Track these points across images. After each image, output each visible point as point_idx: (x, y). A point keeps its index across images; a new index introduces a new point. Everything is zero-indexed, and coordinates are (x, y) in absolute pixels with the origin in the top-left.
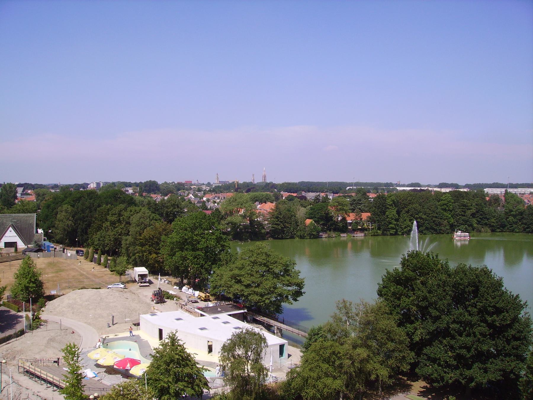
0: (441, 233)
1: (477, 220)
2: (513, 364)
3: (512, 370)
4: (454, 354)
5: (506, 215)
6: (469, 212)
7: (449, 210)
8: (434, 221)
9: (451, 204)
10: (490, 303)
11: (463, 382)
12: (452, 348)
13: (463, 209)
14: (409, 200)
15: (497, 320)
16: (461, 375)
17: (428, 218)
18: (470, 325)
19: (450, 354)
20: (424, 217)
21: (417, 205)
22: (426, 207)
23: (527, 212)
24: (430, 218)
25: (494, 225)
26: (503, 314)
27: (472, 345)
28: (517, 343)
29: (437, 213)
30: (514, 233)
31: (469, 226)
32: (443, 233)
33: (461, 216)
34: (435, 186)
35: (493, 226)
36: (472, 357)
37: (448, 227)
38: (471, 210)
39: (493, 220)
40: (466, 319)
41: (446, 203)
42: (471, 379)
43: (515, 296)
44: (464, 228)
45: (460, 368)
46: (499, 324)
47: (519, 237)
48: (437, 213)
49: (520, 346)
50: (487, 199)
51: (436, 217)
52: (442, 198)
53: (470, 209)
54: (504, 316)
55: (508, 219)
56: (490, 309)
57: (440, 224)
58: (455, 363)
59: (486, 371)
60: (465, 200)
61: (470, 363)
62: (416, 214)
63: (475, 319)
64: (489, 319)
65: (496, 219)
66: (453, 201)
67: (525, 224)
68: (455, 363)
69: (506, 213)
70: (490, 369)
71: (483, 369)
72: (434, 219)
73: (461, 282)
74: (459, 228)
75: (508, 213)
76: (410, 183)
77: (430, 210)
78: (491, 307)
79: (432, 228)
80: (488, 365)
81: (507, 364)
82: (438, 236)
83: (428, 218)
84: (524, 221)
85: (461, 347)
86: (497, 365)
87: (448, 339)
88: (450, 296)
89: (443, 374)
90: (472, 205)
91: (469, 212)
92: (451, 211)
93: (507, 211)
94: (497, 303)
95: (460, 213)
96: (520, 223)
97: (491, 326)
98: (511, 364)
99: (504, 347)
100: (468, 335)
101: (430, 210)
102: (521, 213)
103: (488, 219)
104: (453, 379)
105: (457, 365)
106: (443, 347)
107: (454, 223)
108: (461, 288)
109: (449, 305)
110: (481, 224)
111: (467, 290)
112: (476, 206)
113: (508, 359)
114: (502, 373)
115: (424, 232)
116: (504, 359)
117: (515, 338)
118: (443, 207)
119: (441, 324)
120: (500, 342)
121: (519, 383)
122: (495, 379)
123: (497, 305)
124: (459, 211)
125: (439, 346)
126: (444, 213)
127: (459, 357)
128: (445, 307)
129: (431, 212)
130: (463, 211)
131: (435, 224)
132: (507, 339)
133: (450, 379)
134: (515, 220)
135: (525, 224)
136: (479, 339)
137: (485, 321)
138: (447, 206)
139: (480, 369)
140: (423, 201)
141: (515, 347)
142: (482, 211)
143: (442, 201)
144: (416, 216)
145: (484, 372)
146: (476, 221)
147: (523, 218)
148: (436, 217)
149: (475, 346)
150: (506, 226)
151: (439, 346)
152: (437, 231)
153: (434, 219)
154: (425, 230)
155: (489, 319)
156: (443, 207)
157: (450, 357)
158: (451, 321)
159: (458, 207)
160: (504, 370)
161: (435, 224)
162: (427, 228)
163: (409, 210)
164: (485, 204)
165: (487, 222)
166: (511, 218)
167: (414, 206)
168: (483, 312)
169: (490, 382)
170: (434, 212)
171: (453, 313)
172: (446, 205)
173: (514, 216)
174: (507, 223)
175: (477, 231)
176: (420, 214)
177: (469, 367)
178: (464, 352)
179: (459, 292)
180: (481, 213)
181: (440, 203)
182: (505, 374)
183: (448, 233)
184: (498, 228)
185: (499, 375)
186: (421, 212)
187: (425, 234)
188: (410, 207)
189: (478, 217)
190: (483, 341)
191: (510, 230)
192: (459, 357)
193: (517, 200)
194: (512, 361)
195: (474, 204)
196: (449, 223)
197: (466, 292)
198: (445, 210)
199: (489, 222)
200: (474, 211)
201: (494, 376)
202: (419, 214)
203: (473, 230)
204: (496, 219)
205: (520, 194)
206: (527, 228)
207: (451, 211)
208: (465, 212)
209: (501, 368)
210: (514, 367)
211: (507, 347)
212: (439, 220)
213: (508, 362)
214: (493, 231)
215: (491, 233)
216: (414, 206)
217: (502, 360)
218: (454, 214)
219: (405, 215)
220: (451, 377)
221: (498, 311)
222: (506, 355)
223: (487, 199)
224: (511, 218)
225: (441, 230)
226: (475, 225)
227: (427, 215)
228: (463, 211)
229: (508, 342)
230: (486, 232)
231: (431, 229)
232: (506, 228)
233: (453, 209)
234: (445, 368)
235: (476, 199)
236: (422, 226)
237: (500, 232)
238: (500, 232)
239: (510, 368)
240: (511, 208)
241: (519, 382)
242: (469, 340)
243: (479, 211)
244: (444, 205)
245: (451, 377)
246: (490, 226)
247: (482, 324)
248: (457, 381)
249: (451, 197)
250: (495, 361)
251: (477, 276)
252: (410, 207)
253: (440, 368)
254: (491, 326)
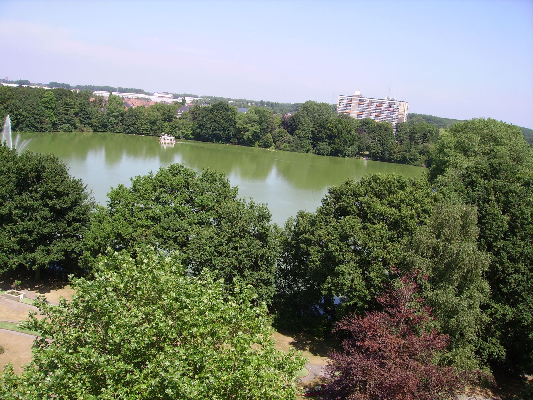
0: (42, 131)
1: (80, 120)
2: (74, 245)
3: (73, 249)
4: (18, 239)
5: (107, 115)
6: (72, 112)
7: (51, 108)
8: (35, 119)
9: (53, 101)
10: (51, 187)
11: (27, 265)
12: (15, 233)
13: (65, 107)
14: (8, 95)
15: (58, 203)
16: (25, 258)
17: (28, 115)
18: (34, 210)
19: (13, 239)
20: (24, 113)
21: (17, 101)
22: (27, 103)
23: (127, 114)
24: (31, 115)
25: (96, 125)
26: (63, 197)
27: (33, 228)
28: (77, 224)
29: (38, 111)
30: (115, 134)
31: (71, 125)
32: (44, 132)
33: (63, 115)
34: (45, 85)
35: (95, 126)
36: (34, 240)
37: (50, 125)
38: (74, 109)
39: (95, 120)
40: (27, 205)
41: (49, 100)
42: (34, 262)
43: (77, 180)
44: (67, 126)
45: (23, 252)
46: (60, 207)
47: (119, 137)
48: (38, 111)
49: (80, 227)
50: (92, 99)
51: (38, 115)
52: (44, 95)
53: (73, 108)
54: (64, 200)
55: (109, 120)
56: (50, 193)
57: (41, 122)
58: (18, 248)
59: (48, 252)
60: (68, 99)
61: (33, 246)
62: (16, 111)
63: (36, 204)
64: (50, 203)
65: (99, 119)
66: (55, 99)
67: (125, 125)
68: (18, 248)
69: (108, 114)
70: (52, 250)
71: (46, 251)
72: (35, 116)
73: (23, 168)
74: (61, 126)
75: (110, 114)
76: (18, 80)
77: (31, 106)
78: (52, 191)
79: (34, 127)
80: (51, 247)
81: (69, 245)
82: (39, 134)
83: (28, 115)
84: (125, 122)
85: (22, 232)
86: (59, 246)
87: (11, 225)
88: (14, 182)
89: (6, 260)
90: (75, 104)
91: (72, 112)
92: (53, 109)
93: (109, 112)
94: (58, 187)
95: (63, 112)
96: (121, 124)
97: (52, 209)
98: (72, 245)
99: (65, 229)
100: (31, 220)
101: (31, 106)
102: (122, 115)
103: (91, 119)
104: (17, 264)
105: (20, 249)
106: (7, 233)
107: (57, 121)
108: (23, 174)
109: (11, 191)
110: (83, 124)
111: (30, 175)
112: (79, 106)
113: (69, 239)
114: (63, 253)
115: (24, 129)
116: (65, 240)
117: (75, 220)
118: (45, 105)
119: (3, 210)
120: (63, 225)
121: (79, 261)
122: (57, 259)
123: (58, 190)
124: (61, 110)
125: (3, 233)
126: (46, 111)
127: (21, 242)
128: (7, 193)
129: (32, 109)
130: (66, 110)
131: (37, 122)
132: (68, 221)
133: (14, 264)
134: (116, 121)
135: (125, 125)
136: (40, 222)
137: (46, 205)
138: (50, 104)
139: (43, 251)
140: (24, 97)
141: (75, 228)
142: (85, 111)
143: (45, 98)
144: (16, 112)
145: (47, 254)
146: (79, 121)
147: (124, 119)
148: (38, 115)
149: (36, 230)
150: (107, 126)
151: (3, 233)
152: (38, 130)
153: (35, 116)
154: (25, 127)
155: (50, 203)
156: (45, 105)
157: (14, 243)
158: (13, 207)
159: (61, 105)
160: (66, 251)
161: (37, 122)
162: (27, 126)
163: (8, 106)
164: (88, 104)
165: (89, 121)
166: (112, 119)
167: (13, 101)
168: (45, 195)
169: (51, 263)
170: (35, 108)
171: (15, 199)
172: (48, 102)
173: (116, 117)
174: (108, 124)
175: (79, 130)
176: (20, 111)
177: (33, 251)
178: (25, 236)
179: (21, 178)
180: (84, 112)
181: (42, 100)
182: (67, 254)
183: (50, 131)
184: (100, 128)
185: (61, 255)
186: (20, 108)
187: (25, 132)
188: (9, 103)
189: (81, 116)
190: (44, 224)
191: (111, 130)
192: (21, 242)
193: (120, 102)
194: (73, 242)
195: (77, 103)
196: (51, 121)
197: (28, 177)
198: (47, 107)
199: (91, 122)
200: (77, 110)
201: (56, 256)
202: (19, 110)
203: (76, 129)
204: (99, 119)
205: (127, 98)
206: (127, 129)
207: (53, 109)
208: (68, 111)
209: (62, 248)
210: (75, 247)
211: (68, 228)
212: (41, 118)
213: (69, 243)
214: (95, 131)
215: (92, 133)
216: (13, 101)
217: (64, 242)
218: (57, 112)
219: (3, 111)
220: (15, 262)
221: (59, 195)
222: (67, 237)
223: (92, 99)
224: (112, 119)
225: (43, 128)
226: (78, 124)
227: (27, 111)
228: (66, 110)
229: (69, 224)
230: (89, 131)
231: (31, 126)
232: (108, 128)
233: (55, 107)
234: (10, 254)
235: (80, 99)
236: (22, 123)
237: (101, 131)
238: (101, 131)
239: (71, 248)
240: (113, 109)
241: (79, 259)
242: (29, 225)
243: (82, 110)
244: (46, 102)
245: (15, 262)
246: (93, 126)
247: (45, 208)
248: (21, 265)
249: (54, 95)
250: (57, 243)
251: (40, 162)
252: (8, 103)
253: (4, 254)
254: (52, 209)
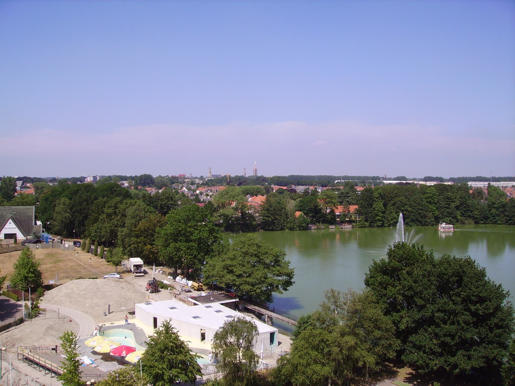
0: (426, 225)
1: (461, 213)
2: (496, 351)
3: (495, 357)
4: (439, 342)
5: (488, 207)
6: (453, 205)
7: (434, 203)
8: (419, 214)
9: (436, 196)
10: (474, 292)
11: (448, 368)
12: (437, 335)
13: (447, 202)
14: (395, 193)
15: (480, 309)
16: (446, 361)
17: (413, 210)
18: (454, 313)
19: (435, 341)
20: (410, 209)
21: (403, 198)
22: (411, 200)
23: (509, 205)
24: (416, 211)
25: (478, 217)
26: (486, 303)
27: (456, 332)
28: (500, 331)
29: (422, 206)
30: (497, 225)
31: (453, 218)
32: (428, 225)
33: (445, 209)
34: (420, 179)
35: (476, 218)
36: (456, 344)
37: (433, 219)
38: (455, 203)
39: (476, 213)
40: (450, 308)
41: (431, 196)
42: (455, 366)
43: (497, 285)
44: (449, 220)
45: (444, 355)
46: (482, 312)
47: (502, 229)
48: (422, 206)
49: (502, 334)
50: (471, 192)
51: (421, 210)
52: (427, 191)
53: (454, 202)
54: (487, 305)
55: (491, 212)
56: (473, 298)
57: (425, 216)
58: (439, 350)
59: (469, 358)
60: (449, 193)
61: (454, 350)
62: (402, 207)
63: (459, 308)
64: (473, 308)
65: (480, 211)
66: (438, 194)
67: (508, 216)
68: (439, 350)
69: (489, 206)
70: (473, 356)
71: (467, 356)
72: (419, 211)
73: (446, 272)
74: (444, 220)
75: (491, 206)
76: (396, 176)
77: (415, 202)
78: (474, 296)
79: (418, 220)
80: (472, 353)
81: (490, 351)
82: (423, 227)
83: (413, 210)
84: (507, 213)
85: (445, 335)
86: (480, 352)
87: (433, 327)
88: (435, 285)
89: (428, 361)
90: (456, 198)
91: (453, 205)
92: (436, 204)
93: (490, 203)
94: (481, 292)
95: (445, 206)
96: (503, 215)
97: (474, 314)
98: (493, 351)
99: (487, 335)
100: (452, 323)
101: (415, 202)
102: (504, 206)
103: (471, 212)
104: (438, 366)
105: (442, 352)
106: (428, 335)
107: (439, 215)
108: (445, 278)
109: (434, 294)
110: (464, 217)
111: (451, 280)
112: (460, 199)
113: (490, 346)
114: (485, 360)
115: (410, 224)
116: (487, 346)
117: (498, 327)
118: (428, 200)
119: (426, 313)
120: (483, 330)
121: (501, 370)
122: (479, 366)
123: (481, 295)
124: (443, 204)
125: (424, 334)
126: (429, 206)
127: (443, 345)
128: (430, 296)
129: (416, 205)
130: (447, 204)
131: (421, 216)
132: (490, 327)
133: (435, 366)
134: (497, 213)
135: (508, 216)
136: (463, 327)
137: (469, 310)
138: (432, 199)
139: (464, 356)
140: (409, 194)
141: (497, 335)
142: (466, 204)
143: (427, 194)
144: (402, 208)
145: (468, 359)
146: (460, 214)
147: (505, 210)
148: (421, 210)
149: (459, 334)
150: (488, 218)
151: (424, 334)
152: (422, 223)
153: (419, 211)
154: (410, 222)
155: (473, 308)
156: (428, 200)
157: (435, 345)
158: (435, 310)
159: (442, 200)
160: (487, 357)
161: (421, 216)
162: (412, 220)
163: (395, 203)
164: (469, 197)
165: (470, 214)
166: (493, 211)
167: (400, 198)
168: (466, 301)
169: (473, 368)
170: (419, 204)
171: (437, 302)
172: (431, 198)
173: (497, 209)
174: (489, 216)
175: (461, 223)
176: (406, 207)
177: (453, 355)
178: (448, 339)
179: (443, 282)
180: (465, 205)
181: (425, 196)
182: (488, 360)
183: (433, 225)
184: (482, 220)
185: (482, 361)
186: (407, 205)
187: (411, 226)
188: (396, 200)
189: (462, 209)
190: (467, 329)
191: (493, 222)
192: (443, 345)
193: (500, 193)
194: (495, 349)
195: (458, 197)
196: (434, 215)
197: (450, 282)
198: (430, 202)
199: (472, 214)
200: (458, 203)
201: (477, 363)
202: (405, 207)
203: (457, 222)
204: (480, 211)
205: (502, 187)
206: (510, 220)
207: (436, 204)
208: (449, 205)
209: (484, 355)
210: (497, 355)
211: (490, 335)
212: (424, 212)
213: (491, 349)
214: (476, 223)
215: (474, 225)
216: (400, 198)
217: (485, 348)
218: (439, 207)
219: (392, 207)
220: (436, 364)
221: (481, 300)
222: (489, 343)
223: (471, 192)
224: (493, 211)
225: (426, 222)
226: (459, 217)
227: (412, 207)
228: (447, 204)
229: (491, 330)
230: (470, 224)
231: (416, 221)
232: (489, 220)
233: (438, 202)
234: (430, 355)
235: (460, 192)
236: (408, 218)
237: (483, 223)
238: (483, 223)
239: (493, 355)
240: (494, 201)
241: (502, 368)
242: (453, 328)
243: (463, 203)
244: (429, 197)
245: (436, 364)
246: (474, 218)
247: (466, 313)
248: (441, 367)
249: (436, 191)
250: (478, 348)
251: (461, 267)
252: (396, 200)
253: (425, 355)
254: (474, 314)
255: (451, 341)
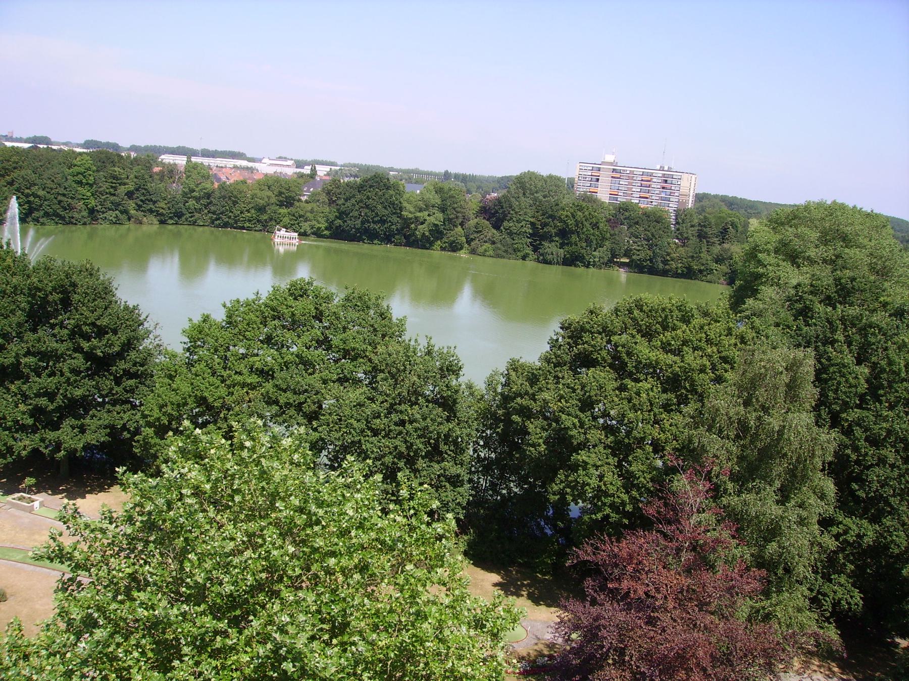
0: (72, 223)
1: (136, 204)
2: (126, 417)
3: (124, 425)
4: (30, 407)
5: (183, 197)
6: (122, 190)
7: (87, 184)
8: (60, 202)
9: (91, 173)
10: (87, 318)
11: (46, 451)
12: (25, 397)
13: (112, 183)
14: (14, 162)
15: (98, 346)
16: (43, 440)
17: (48, 196)
18: (58, 357)
19: (22, 407)
20: (41, 193)
21: (30, 172)
22: (46, 176)
23: (217, 194)
24: (53, 196)
25: (164, 212)
26: (107, 336)
27: (57, 388)
28: (132, 382)
29: (65, 188)
30: (196, 227)
31: (122, 212)
32: (76, 224)
33: (108, 196)
34: (77, 144)
35: (162, 214)
36: (59, 408)
37: (85, 213)
38: (127, 186)
39: (162, 204)
40: (47, 348)
41: (83, 170)
42: (58, 446)
43: (131, 306)
44: (114, 215)
45: (38, 429)
46: (102, 352)
47: (204, 233)
48: (65, 188)
49: (137, 387)
50: (156, 169)
51: (64, 195)
52: (75, 162)
53: (125, 184)
54: (108, 340)
55: (187, 204)
56: (85, 328)
57: (71, 208)
58: (30, 421)
59: (83, 430)
60: (116, 169)
61: (56, 419)
62: (27, 188)
63: (62, 348)
64: (85, 345)
65: (168, 203)
66: (95, 168)
67: (214, 213)
68: (30, 421)
69: (185, 194)
70: (89, 426)
71: (78, 428)
72: (60, 198)
73: (40, 286)
74: (105, 215)
75: (188, 194)
76: (32, 135)
77: (53, 181)
78: (88, 325)
79: (58, 215)
80: (87, 421)
81: (117, 416)
82: (67, 228)
83: (48, 196)
84: (212, 208)
85: (38, 395)
86: (100, 419)
87: (19, 382)
88: (23, 310)
89: (11, 442)
90: (128, 178)
91: (122, 190)
92: (91, 185)
93: (187, 190)
94: (99, 319)
95: (107, 191)
96: (206, 211)
97: (89, 356)
98: (123, 417)
99: (112, 389)
100: (52, 374)
101: (53, 181)
102: (208, 195)
103: (155, 202)
104: (29, 449)
105: (34, 425)
106: (12, 396)
107: (96, 206)
108: (39, 297)
109: (20, 325)
110: (142, 211)
111: (50, 298)
112: (135, 180)
113: (118, 408)
114: (108, 430)
115: (41, 220)
116: (111, 408)
117: (129, 374)
118: (76, 178)
119: (5, 358)
120: (107, 383)
121: (134, 444)
122: (98, 441)
123: (98, 323)
124: (105, 187)
125: (5, 396)
126: (79, 189)
127: (37, 412)
128: (12, 328)
129: (55, 186)
130: (112, 187)
131: (63, 207)
132: (115, 377)
133: (24, 449)
134: (198, 206)
135: (214, 213)
136: (69, 379)
137: (78, 349)
138: (84, 177)
139: (73, 428)
140: (41, 166)
141: (128, 388)
142: (145, 189)
143: (76, 168)
144: (27, 191)
145: (80, 432)
146: (134, 205)
147: (211, 202)
148: (64, 195)
149: (61, 391)
150: (183, 215)
151: (5, 396)
152: (65, 221)
153: (60, 198)
154: (43, 217)
155: (85, 345)
156: (76, 178)
157: (24, 413)
158: (22, 352)
159: (104, 179)
160: (112, 427)
161: (63, 207)
162: (47, 215)
163: (13, 181)
164: (151, 177)
165: (152, 207)
166: (191, 203)
167: (23, 172)
168: (76, 332)
169: (87, 447)
170: (59, 185)
171: (25, 338)
172: (82, 174)
173: (198, 199)
174: (184, 211)
175: (135, 222)
176: (34, 189)
177: (56, 427)
178: (43, 401)
179: (36, 304)
180: (144, 191)
181: (71, 170)
182: (114, 432)
183: (85, 224)
184: (171, 218)
185: (103, 434)
186: (35, 185)
187: (43, 224)
188: (16, 175)
189: (138, 198)
190: (76, 381)
191: (190, 222)
192: (37, 412)
193: (205, 174)
194: (125, 412)
195: (132, 176)
196: (87, 205)
197: (48, 302)
198: (80, 183)
199: (156, 207)
200: (131, 187)
201: (96, 436)
202: (32, 188)
203: (129, 219)
204: (168, 203)
205: (217, 166)
206: (217, 219)
207: (91, 185)
208: (115, 188)
209: (106, 422)
210: (128, 421)
211: (116, 389)
212: (70, 200)
213: (118, 413)
214: (162, 222)
215: (158, 226)
216: (23, 172)
217: (109, 411)
218: (96, 191)
219: (6, 188)
220: (25, 446)
221: (101, 332)
222: (114, 403)
223: (156, 169)
224: (191, 203)
225: (73, 218)
226: (132, 212)
227: (47, 189)
228: (112, 187)
229: (118, 381)
230: (151, 224)
231: (54, 215)
232: (183, 218)
233: (94, 183)
234: (17, 432)
235: (136, 168)
236: (38, 210)
237: (173, 224)
238: (173, 224)
239: (122, 422)
240: (192, 186)
241: (135, 442)
242: (50, 382)
243: (140, 187)
244: (78, 173)
245: (25, 446)
246: (158, 214)
247: (76, 355)
248: (35, 451)
249: (91, 162)
250: (98, 414)
251: (68, 276)
252: (14, 175)
253: (7, 432)
254: (89, 356)
255: (153, 441)
